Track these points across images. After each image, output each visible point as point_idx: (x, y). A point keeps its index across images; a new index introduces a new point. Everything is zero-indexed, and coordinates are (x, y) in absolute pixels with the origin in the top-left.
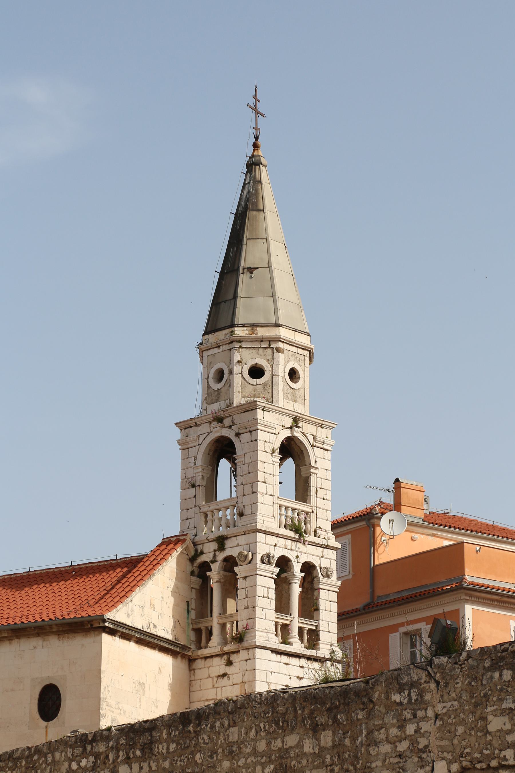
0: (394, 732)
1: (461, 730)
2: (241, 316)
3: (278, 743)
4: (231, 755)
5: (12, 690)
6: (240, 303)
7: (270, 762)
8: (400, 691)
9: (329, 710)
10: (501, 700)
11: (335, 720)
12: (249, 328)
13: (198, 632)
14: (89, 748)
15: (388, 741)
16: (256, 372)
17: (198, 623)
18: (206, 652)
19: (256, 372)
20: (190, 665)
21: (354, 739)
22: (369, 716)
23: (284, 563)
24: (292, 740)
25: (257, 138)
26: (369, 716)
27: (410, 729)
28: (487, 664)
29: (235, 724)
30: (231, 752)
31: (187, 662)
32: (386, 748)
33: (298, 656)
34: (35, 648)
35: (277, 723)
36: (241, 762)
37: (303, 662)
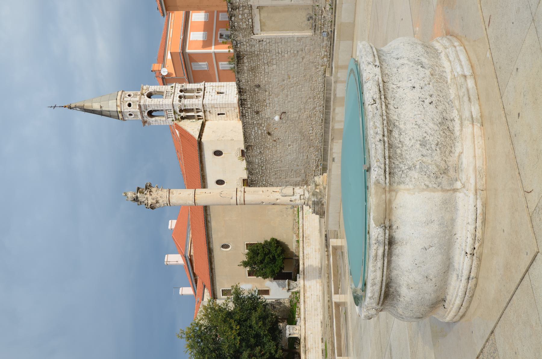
0: (245, 46)
2: (115, 109)
4: (248, 82)
6: (110, 109)
16: (130, 105)
19: (130, 105)
23: (180, 97)
24: (245, 68)
37: (205, 92)
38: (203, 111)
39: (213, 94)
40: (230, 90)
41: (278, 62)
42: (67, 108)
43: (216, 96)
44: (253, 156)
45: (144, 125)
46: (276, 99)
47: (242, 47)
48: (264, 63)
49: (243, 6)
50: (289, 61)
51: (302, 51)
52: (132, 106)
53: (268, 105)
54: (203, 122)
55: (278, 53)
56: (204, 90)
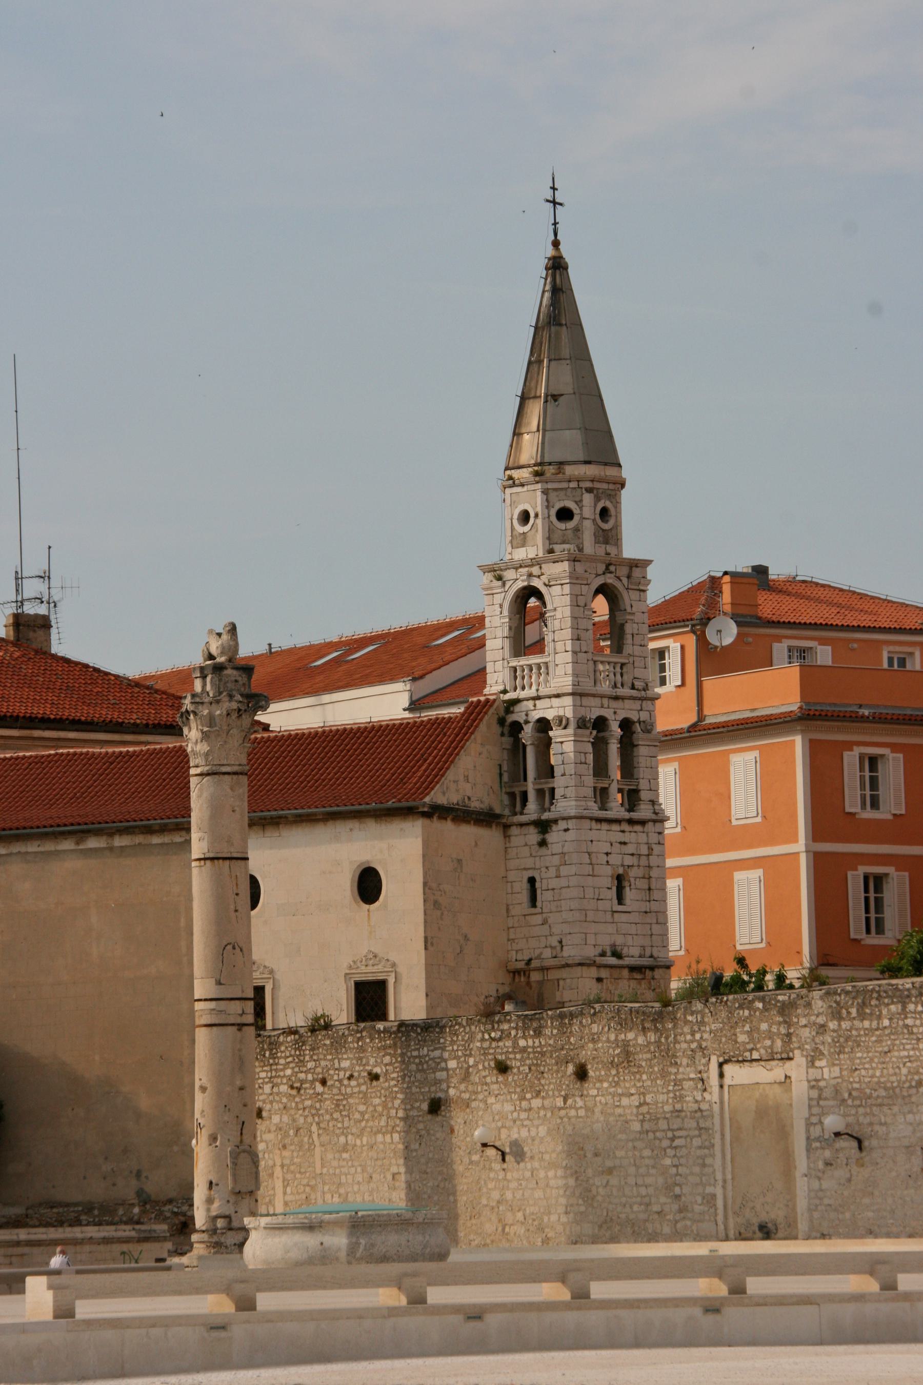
0: (689, 1037)
1: (724, 1040)
3: (623, 1036)
4: (593, 1041)
5: (330, 872)
7: (618, 1046)
8: (692, 1015)
9: (652, 1021)
10: (744, 1026)
11: (655, 1026)
12: (556, 467)
13: (512, 795)
14: (496, 1026)
15: (685, 1042)
17: (511, 787)
18: (523, 819)
20: (504, 832)
21: (667, 1038)
22: (675, 1026)
24: (630, 1036)
25: (556, 234)
26: (675, 1026)
27: (698, 1036)
28: (737, 1005)
29: (595, 1022)
30: (593, 1039)
31: (502, 828)
32: (684, 1046)
33: (618, 821)
34: (351, 830)
35: (621, 1025)
36: (600, 1045)
38: (546, 816)
39: (615, 859)
40: (633, 929)
41: (651, 1135)
42: (550, 252)
43: (608, 871)
44: (362, 1049)
45: (486, 569)
46: (543, 1130)
47: (686, 1029)
48: (644, 1094)
49: (789, 1035)
50: (653, 1171)
51: (680, 1211)
52: (561, 526)
53: (524, 1104)
54: (499, 816)
55: (672, 1140)
56: (631, 822)
